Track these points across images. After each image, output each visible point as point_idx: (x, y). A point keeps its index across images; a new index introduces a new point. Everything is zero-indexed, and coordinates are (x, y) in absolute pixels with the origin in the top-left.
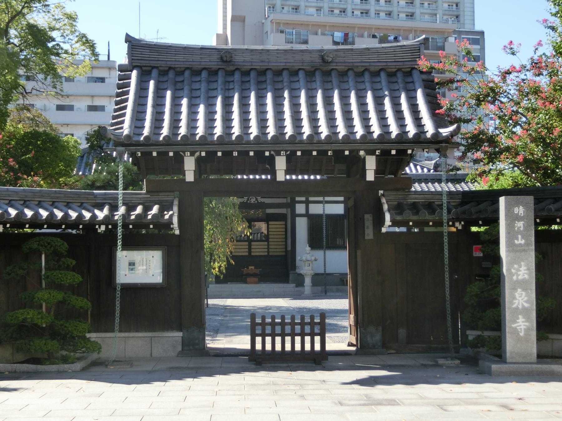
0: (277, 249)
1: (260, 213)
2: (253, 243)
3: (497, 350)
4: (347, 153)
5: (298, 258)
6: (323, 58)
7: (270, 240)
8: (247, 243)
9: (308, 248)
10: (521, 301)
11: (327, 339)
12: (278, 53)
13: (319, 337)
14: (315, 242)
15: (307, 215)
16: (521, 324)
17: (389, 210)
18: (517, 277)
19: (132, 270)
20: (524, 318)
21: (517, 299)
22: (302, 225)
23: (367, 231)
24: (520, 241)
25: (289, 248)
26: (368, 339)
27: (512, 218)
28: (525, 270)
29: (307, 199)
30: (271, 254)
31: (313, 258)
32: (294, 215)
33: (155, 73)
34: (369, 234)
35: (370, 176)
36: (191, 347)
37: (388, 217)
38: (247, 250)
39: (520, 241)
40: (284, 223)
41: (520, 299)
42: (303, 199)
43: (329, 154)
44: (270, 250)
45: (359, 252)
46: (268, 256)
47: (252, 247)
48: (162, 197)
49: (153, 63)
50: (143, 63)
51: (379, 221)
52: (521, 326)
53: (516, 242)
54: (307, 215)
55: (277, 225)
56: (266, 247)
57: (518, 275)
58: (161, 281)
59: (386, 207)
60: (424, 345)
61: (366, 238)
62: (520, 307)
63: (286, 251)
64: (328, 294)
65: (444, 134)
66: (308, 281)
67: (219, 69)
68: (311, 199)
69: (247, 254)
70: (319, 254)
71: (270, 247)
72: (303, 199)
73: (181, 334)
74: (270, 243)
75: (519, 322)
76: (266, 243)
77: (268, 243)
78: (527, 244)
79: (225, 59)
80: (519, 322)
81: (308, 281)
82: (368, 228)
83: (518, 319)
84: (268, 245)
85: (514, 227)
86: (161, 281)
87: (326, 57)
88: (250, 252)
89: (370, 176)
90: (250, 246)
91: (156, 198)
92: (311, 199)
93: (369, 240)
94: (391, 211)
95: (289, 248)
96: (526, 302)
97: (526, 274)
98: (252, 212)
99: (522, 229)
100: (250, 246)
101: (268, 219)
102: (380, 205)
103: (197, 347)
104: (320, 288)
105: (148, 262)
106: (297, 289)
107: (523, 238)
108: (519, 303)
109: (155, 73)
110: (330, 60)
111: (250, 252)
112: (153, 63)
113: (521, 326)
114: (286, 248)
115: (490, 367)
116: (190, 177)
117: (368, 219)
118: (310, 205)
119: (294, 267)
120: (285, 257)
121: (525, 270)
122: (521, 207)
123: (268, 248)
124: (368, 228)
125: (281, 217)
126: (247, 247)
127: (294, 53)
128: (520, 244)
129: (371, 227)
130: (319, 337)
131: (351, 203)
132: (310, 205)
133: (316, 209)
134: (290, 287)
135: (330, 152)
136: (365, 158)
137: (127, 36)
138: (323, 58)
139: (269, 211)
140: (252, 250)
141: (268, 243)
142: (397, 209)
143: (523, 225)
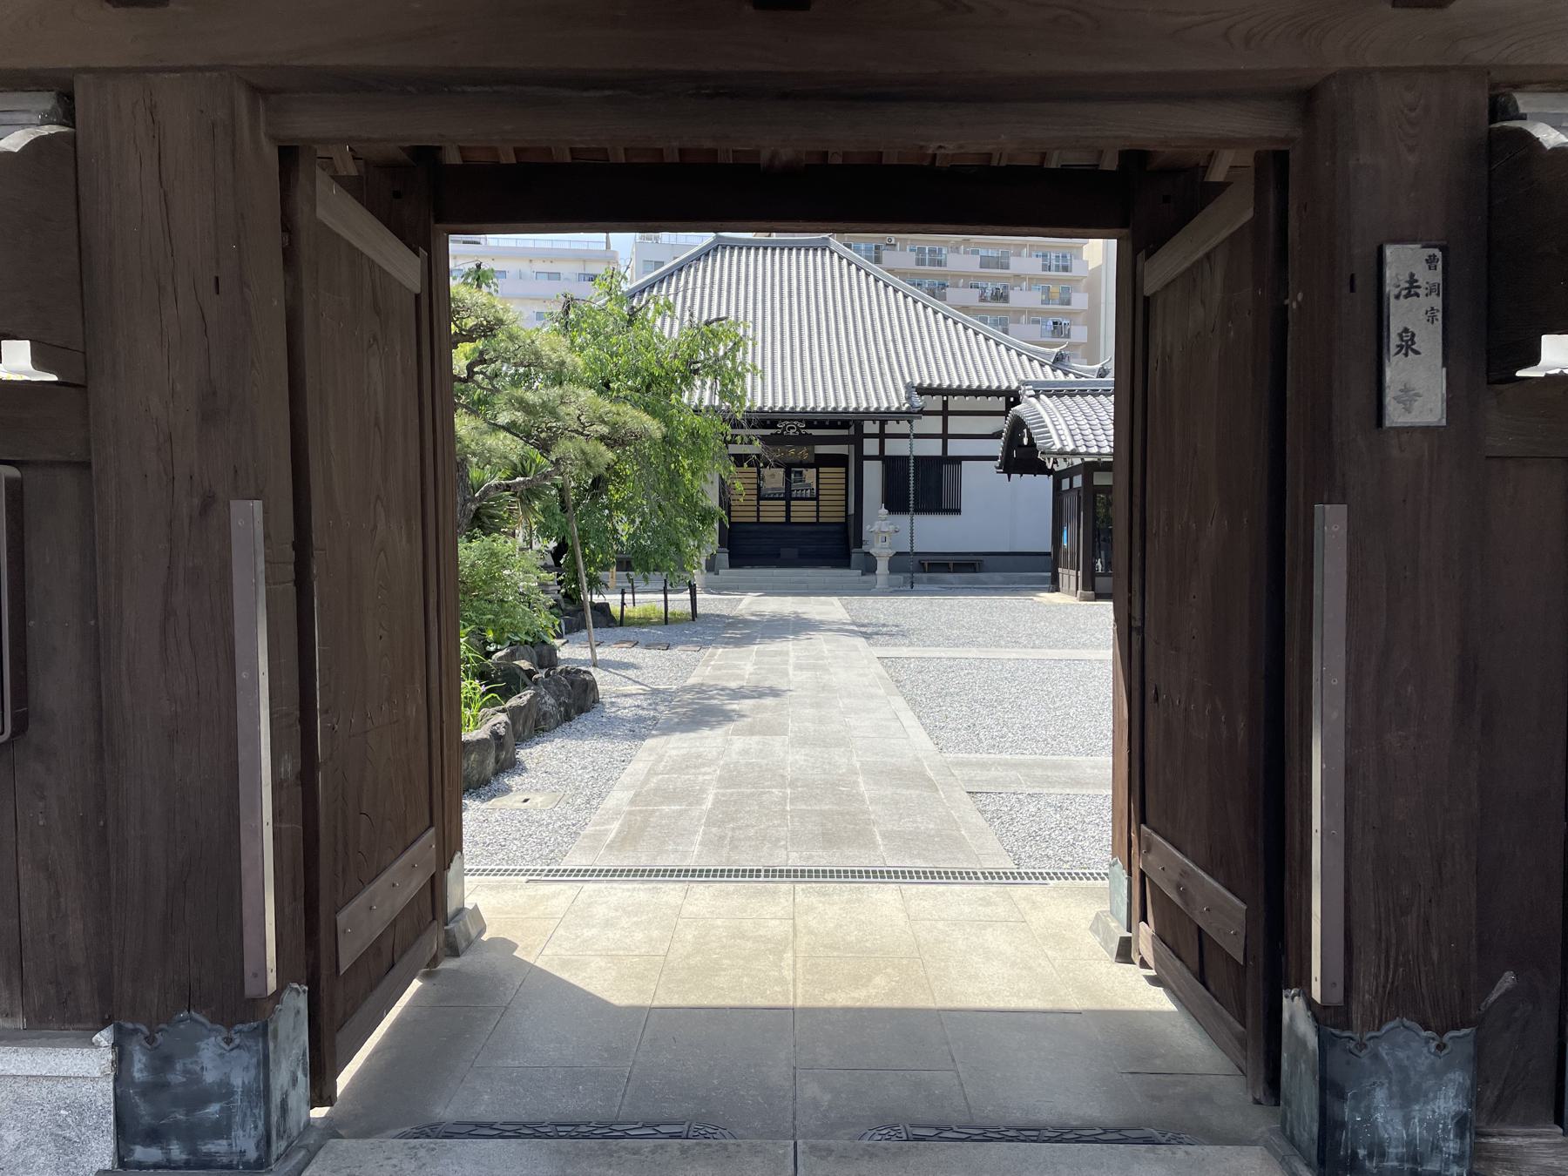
0: (832, 513)
1: (804, 453)
5: (866, 527)
9: (884, 511)
14: (895, 502)
15: (881, 456)
22: (873, 474)
23: (1396, 371)
25: (852, 511)
26: (1379, 1117)
31: (892, 528)
32: (861, 458)
36: (177, 1152)
54: (881, 456)
55: (832, 475)
61: (1395, 415)
63: (847, 516)
64: (916, 587)
66: (882, 566)
70: (903, 520)
81: (882, 566)
82: (1408, 345)
88: (788, 516)
90: (788, 506)
93: (1410, 430)
98: (792, 452)
100: (788, 506)
101: (822, 461)
103: (217, 1147)
104: (900, 578)
111: (788, 516)
114: (847, 506)
119: (859, 542)
120: (845, 524)
124: (1408, 345)
125: (840, 461)
129: (1430, 340)
133: (895, 448)
134: (852, 574)
139: (822, 449)
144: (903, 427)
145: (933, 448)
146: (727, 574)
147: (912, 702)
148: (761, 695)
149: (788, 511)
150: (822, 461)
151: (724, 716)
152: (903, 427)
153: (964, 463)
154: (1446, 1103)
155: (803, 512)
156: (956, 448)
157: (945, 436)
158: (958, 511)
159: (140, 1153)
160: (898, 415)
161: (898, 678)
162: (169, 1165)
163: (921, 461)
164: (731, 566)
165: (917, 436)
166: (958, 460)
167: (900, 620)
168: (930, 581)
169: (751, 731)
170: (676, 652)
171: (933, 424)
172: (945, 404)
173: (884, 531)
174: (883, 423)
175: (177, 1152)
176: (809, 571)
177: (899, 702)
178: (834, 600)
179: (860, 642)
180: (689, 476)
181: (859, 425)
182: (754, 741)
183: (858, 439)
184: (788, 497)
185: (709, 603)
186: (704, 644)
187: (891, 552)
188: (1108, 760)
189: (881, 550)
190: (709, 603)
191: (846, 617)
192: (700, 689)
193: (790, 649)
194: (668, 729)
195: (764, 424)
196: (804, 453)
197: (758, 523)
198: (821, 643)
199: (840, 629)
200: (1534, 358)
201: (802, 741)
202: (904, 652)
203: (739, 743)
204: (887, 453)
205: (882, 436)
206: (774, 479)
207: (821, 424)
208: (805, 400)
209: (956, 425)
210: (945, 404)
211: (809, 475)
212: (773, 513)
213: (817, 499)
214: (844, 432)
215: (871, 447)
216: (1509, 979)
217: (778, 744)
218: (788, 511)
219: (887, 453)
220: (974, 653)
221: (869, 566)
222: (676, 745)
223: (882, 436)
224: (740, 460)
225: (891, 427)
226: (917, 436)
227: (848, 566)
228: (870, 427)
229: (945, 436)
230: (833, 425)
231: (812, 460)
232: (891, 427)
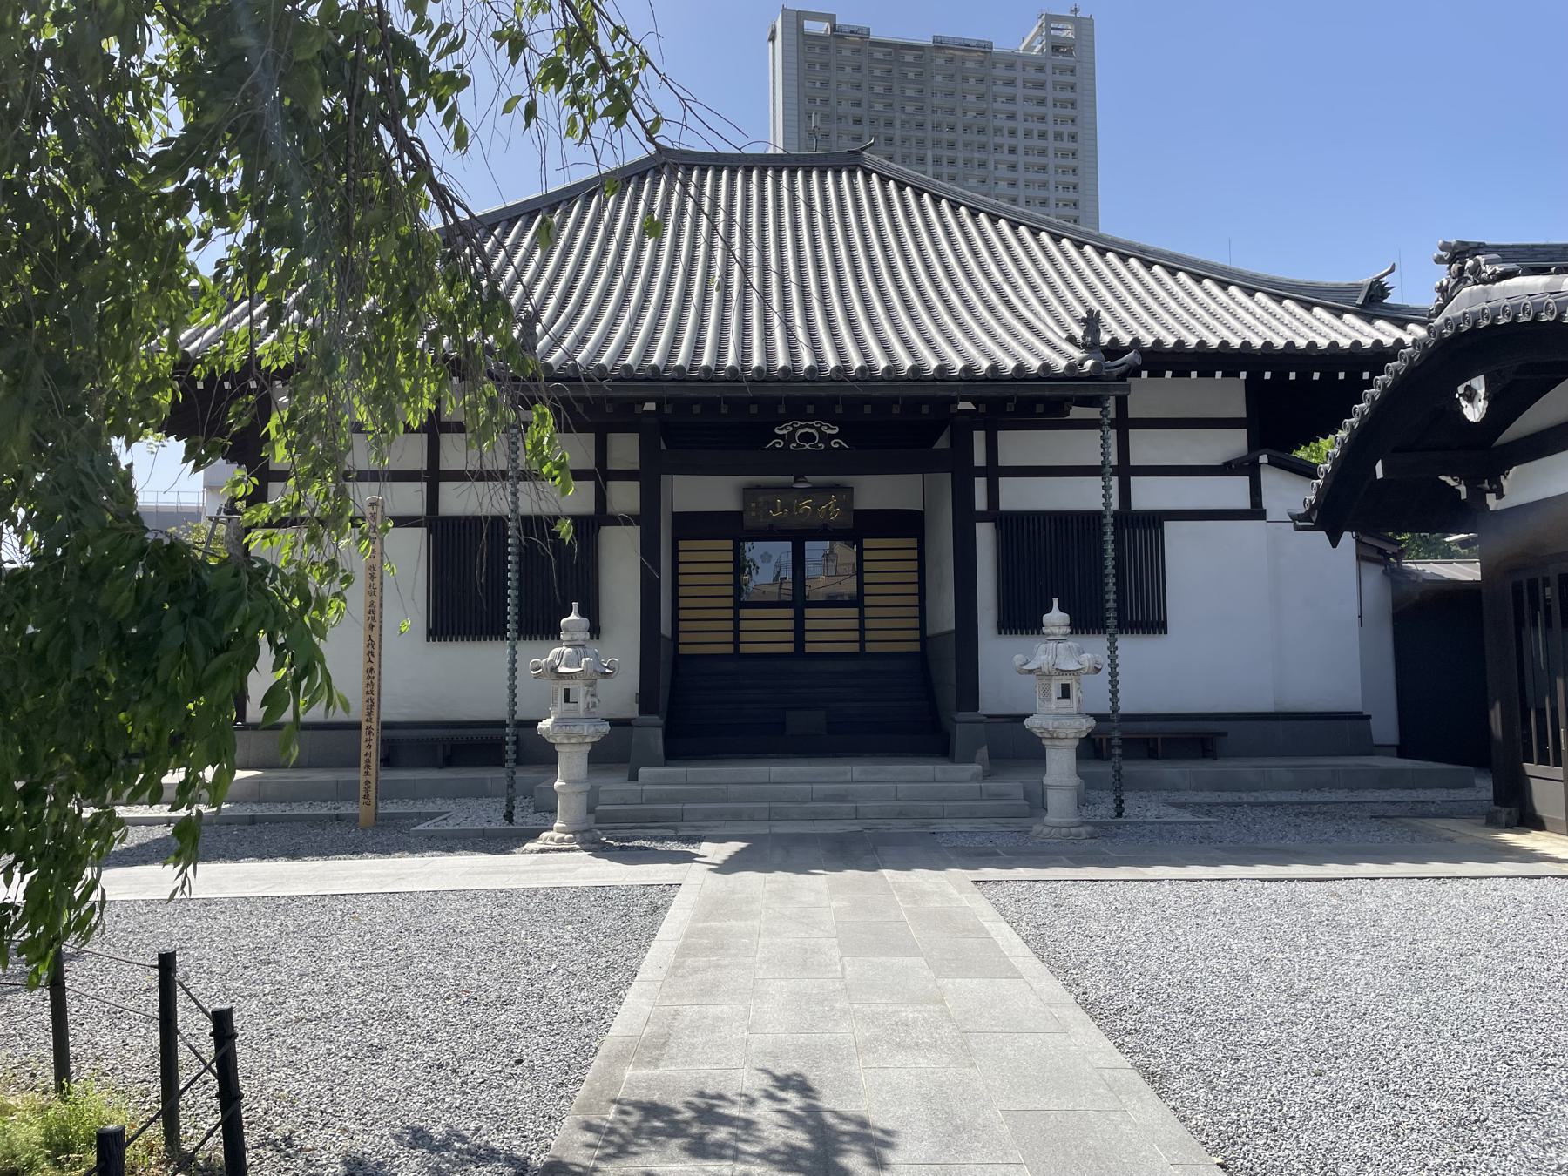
0: (891, 634)
2: (809, 612)
4: (650, 407)
7: (868, 601)
8: (789, 612)
13: (984, 480)
29: (981, 472)
30: (870, 648)
38: (790, 636)
40: (913, 542)
42: (980, 485)
44: (869, 636)
46: (861, 655)
47: (808, 625)
55: (886, 552)
56: (855, 624)
66: (1061, 765)
68: (980, 459)
69: (789, 648)
71: (869, 624)
72: (980, 485)
74: (868, 612)
76: (854, 612)
77: (861, 612)
84: (862, 618)
88: (799, 641)
90: (799, 620)
92: (980, 459)
100: (799, 620)
106: (992, 786)
111: (799, 641)
118: (1135, 481)
123: (862, 630)
125: (908, 524)
126: (790, 625)
130: (984, 480)
132: (1135, 481)
140: (808, 636)
141: (861, 612)
145: (1086, 495)
149: (799, 630)
153: (1170, 527)
156: (1148, 495)
158: (1156, 624)
166: (1156, 520)
184: (799, 602)
188: (938, 767)
197: (737, 656)
200: (1062, 609)
204: (1005, 505)
208: (839, 349)
209: (1146, 447)
212: (768, 635)
218: (799, 630)
219: (1005, 505)
229: (1125, 471)
231: (849, 522)
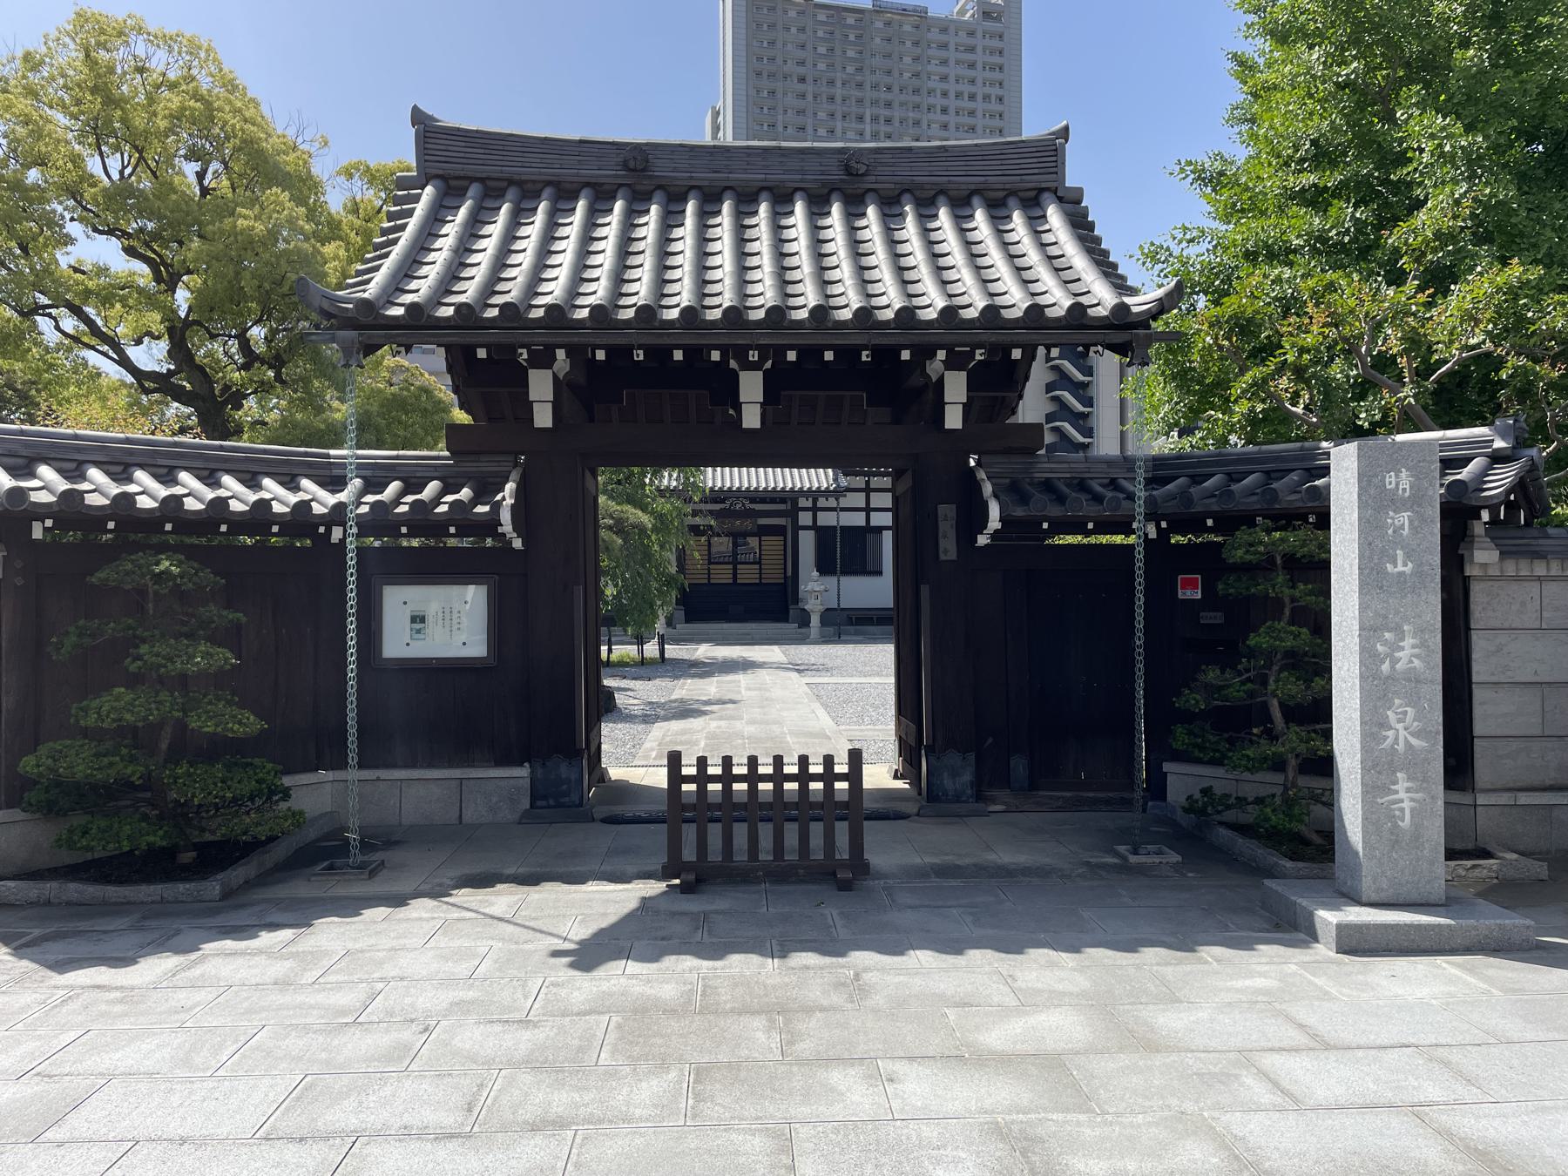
0: (773, 575)
1: (748, 524)
3: (1309, 845)
5: (802, 587)
6: (848, 170)
9: (816, 573)
10: (1402, 733)
11: (867, 839)
12: (749, 155)
14: (825, 566)
15: (814, 527)
16: (1402, 795)
17: (996, 496)
18: (1393, 667)
19: (418, 632)
20: (1409, 779)
21: (1391, 728)
22: (807, 541)
23: (943, 544)
24: (1401, 566)
25: (789, 573)
27: (1374, 500)
28: (1413, 647)
32: (797, 528)
33: (474, 189)
34: (948, 548)
35: (953, 419)
36: (551, 802)
37: (994, 511)
39: (1402, 567)
41: (1400, 726)
43: (864, 358)
45: (925, 590)
48: (487, 466)
49: (470, 169)
50: (451, 169)
51: (974, 516)
52: (1402, 801)
53: (1389, 567)
54: (814, 527)
55: (772, 543)
57: (1395, 661)
58: (484, 653)
59: (988, 489)
60: (1068, 794)
61: (943, 557)
62: (1401, 747)
65: (1135, 309)
66: (815, 620)
67: (621, 185)
70: (831, 581)
73: (523, 772)
75: (1397, 792)
78: (1418, 573)
79: (632, 164)
80: (1397, 792)
81: (815, 620)
83: (1395, 783)
85: (1384, 527)
86: (484, 653)
87: (853, 164)
89: (953, 419)
90: (735, 569)
91: (470, 467)
94: (1002, 497)
95: (789, 573)
96: (1416, 734)
97: (1417, 656)
99: (1406, 532)
100: (735, 569)
101: (763, 531)
102: (976, 487)
105: (455, 615)
107: (1408, 556)
108: (1397, 739)
109: (474, 189)
110: (863, 169)
112: (471, 170)
113: (1402, 801)
115: (1311, 915)
116: (543, 418)
117: (947, 513)
119: (796, 600)
120: (784, 585)
121: (1413, 647)
122: (1404, 473)
125: (779, 531)
127: (783, 155)
128: (1401, 574)
129: (952, 534)
131: (906, 483)
133: (826, 519)
135: (865, 353)
136: (941, 380)
137: (415, 109)
138: (848, 170)
142: (1012, 491)
143: (1411, 522)
144: (832, 503)
145: (858, 520)
146: (682, 628)
147: (825, 706)
148: (724, 703)
150: (763, 531)
151: (704, 713)
152: (832, 503)
154: (967, 777)
155: (748, 574)
157: (868, 510)
159: (539, 803)
160: (827, 493)
161: (817, 692)
162: (549, 807)
163: (847, 530)
164: (687, 621)
165: (843, 509)
167: (826, 661)
168: (856, 633)
169: (721, 719)
170: (657, 682)
171: (858, 500)
172: (868, 483)
173: (816, 590)
174: (815, 501)
175: (551, 802)
176: (753, 625)
177: (817, 706)
178: (775, 648)
179: (794, 675)
180: (656, 547)
181: (795, 501)
182: (722, 723)
183: (795, 511)
185: (672, 651)
186: (677, 677)
187: (822, 608)
189: (814, 606)
190: (672, 651)
191: (783, 659)
192: (682, 701)
193: (742, 679)
194: (666, 719)
195: (715, 501)
196: (748, 524)
197: (710, 584)
198: (763, 675)
199: (779, 667)
201: (752, 722)
202: (825, 680)
203: (714, 724)
205: (815, 510)
206: (723, 545)
207: (763, 501)
210: (868, 483)
211: (753, 542)
212: (722, 575)
213: (759, 563)
214: (782, 507)
215: (805, 518)
216: (990, 740)
217: (738, 725)
220: (877, 680)
221: (805, 621)
222: (676, 725)
223: (815, 510)
224: (695, 530)
225: (822, 503)
226: (843, 509)
227: (787, 620)
228: (803, 503)
230: (773, 501)
232: (822, 503)
